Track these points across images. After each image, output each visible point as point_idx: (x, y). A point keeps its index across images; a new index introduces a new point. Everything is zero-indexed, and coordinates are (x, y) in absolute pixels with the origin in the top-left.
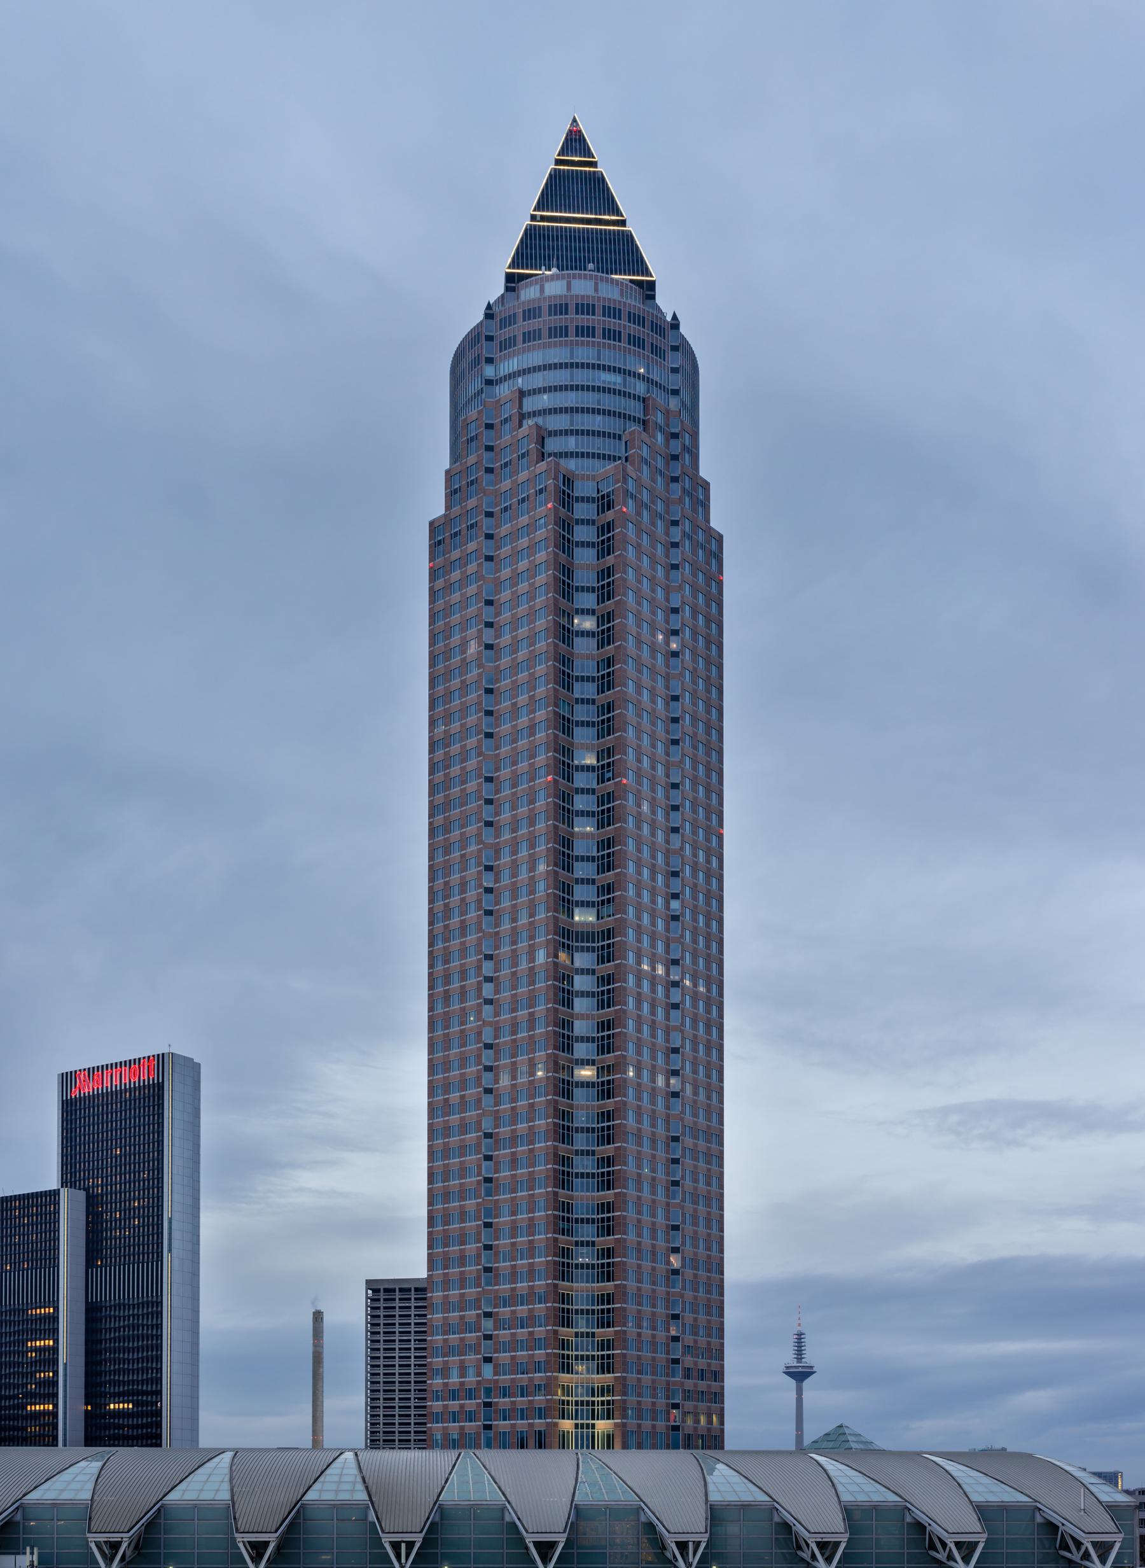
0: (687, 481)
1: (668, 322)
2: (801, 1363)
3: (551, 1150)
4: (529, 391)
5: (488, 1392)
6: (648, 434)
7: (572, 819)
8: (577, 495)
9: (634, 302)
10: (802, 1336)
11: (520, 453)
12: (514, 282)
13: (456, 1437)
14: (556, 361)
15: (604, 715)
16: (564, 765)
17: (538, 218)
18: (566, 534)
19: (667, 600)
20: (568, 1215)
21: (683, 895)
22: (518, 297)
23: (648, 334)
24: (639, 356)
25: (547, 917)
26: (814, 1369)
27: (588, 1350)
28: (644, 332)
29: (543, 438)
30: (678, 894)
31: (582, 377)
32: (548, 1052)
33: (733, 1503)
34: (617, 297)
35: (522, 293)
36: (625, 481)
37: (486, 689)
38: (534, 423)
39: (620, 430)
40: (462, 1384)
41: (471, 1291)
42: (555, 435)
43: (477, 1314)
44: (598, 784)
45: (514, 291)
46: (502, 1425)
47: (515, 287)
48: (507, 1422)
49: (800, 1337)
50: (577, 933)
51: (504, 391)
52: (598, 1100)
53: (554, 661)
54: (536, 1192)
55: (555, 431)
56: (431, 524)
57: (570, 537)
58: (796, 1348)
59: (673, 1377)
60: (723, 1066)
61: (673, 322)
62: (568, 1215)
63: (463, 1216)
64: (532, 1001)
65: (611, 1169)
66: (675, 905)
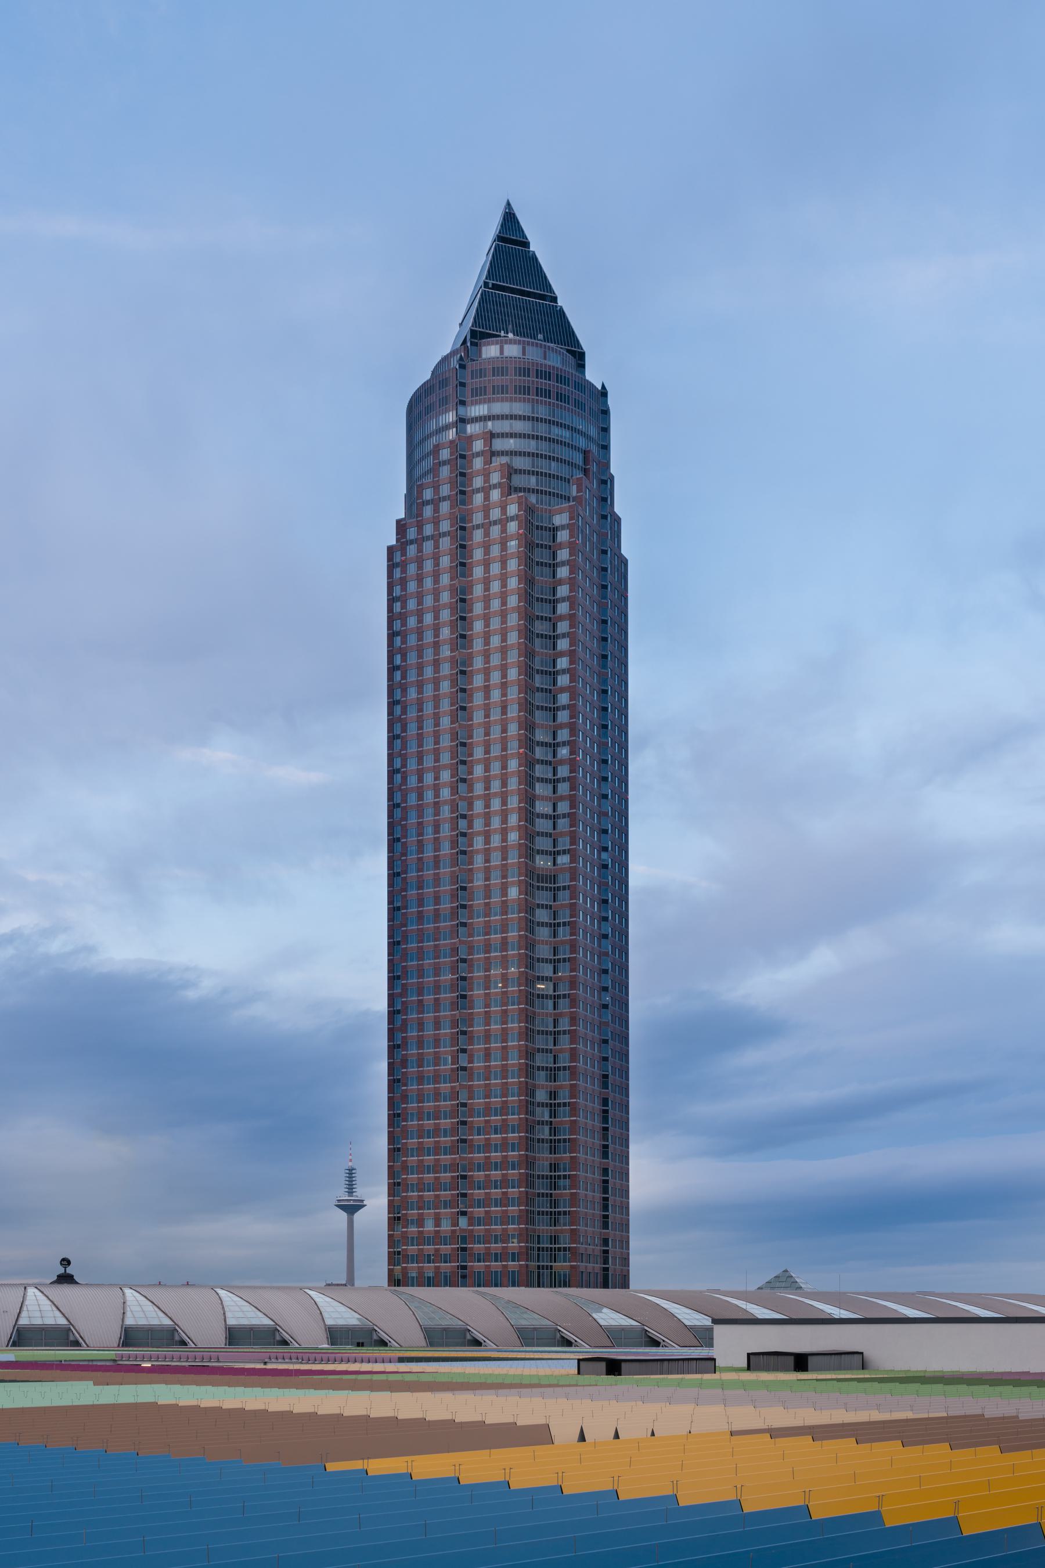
2: (352, 1196)
3: (524, 1049)
5: (464, 1239)
9: (571, 370)
10: (354, 1171)
13: (431, 1275)
14: (521, 413)
17: (490, 286)
24: (572, 412)
25: (519, 862)
26: (365, 1203)
27: (547, 1208)
28: (561, 388)
29: (511, 474)
32: (521, 970)
33: (344, 1327)
34: (559, 365)
35: (484, 349)
39: (569, 475)
40: (453, 1231)
41: (446, 1158)
45: (477, 346)
46: (478, 1266)
47: (477, 343)
51: (470, 429)
61: (603, 391)
63: (437, 1095)
64: (504, 928)
66: (604, 855)
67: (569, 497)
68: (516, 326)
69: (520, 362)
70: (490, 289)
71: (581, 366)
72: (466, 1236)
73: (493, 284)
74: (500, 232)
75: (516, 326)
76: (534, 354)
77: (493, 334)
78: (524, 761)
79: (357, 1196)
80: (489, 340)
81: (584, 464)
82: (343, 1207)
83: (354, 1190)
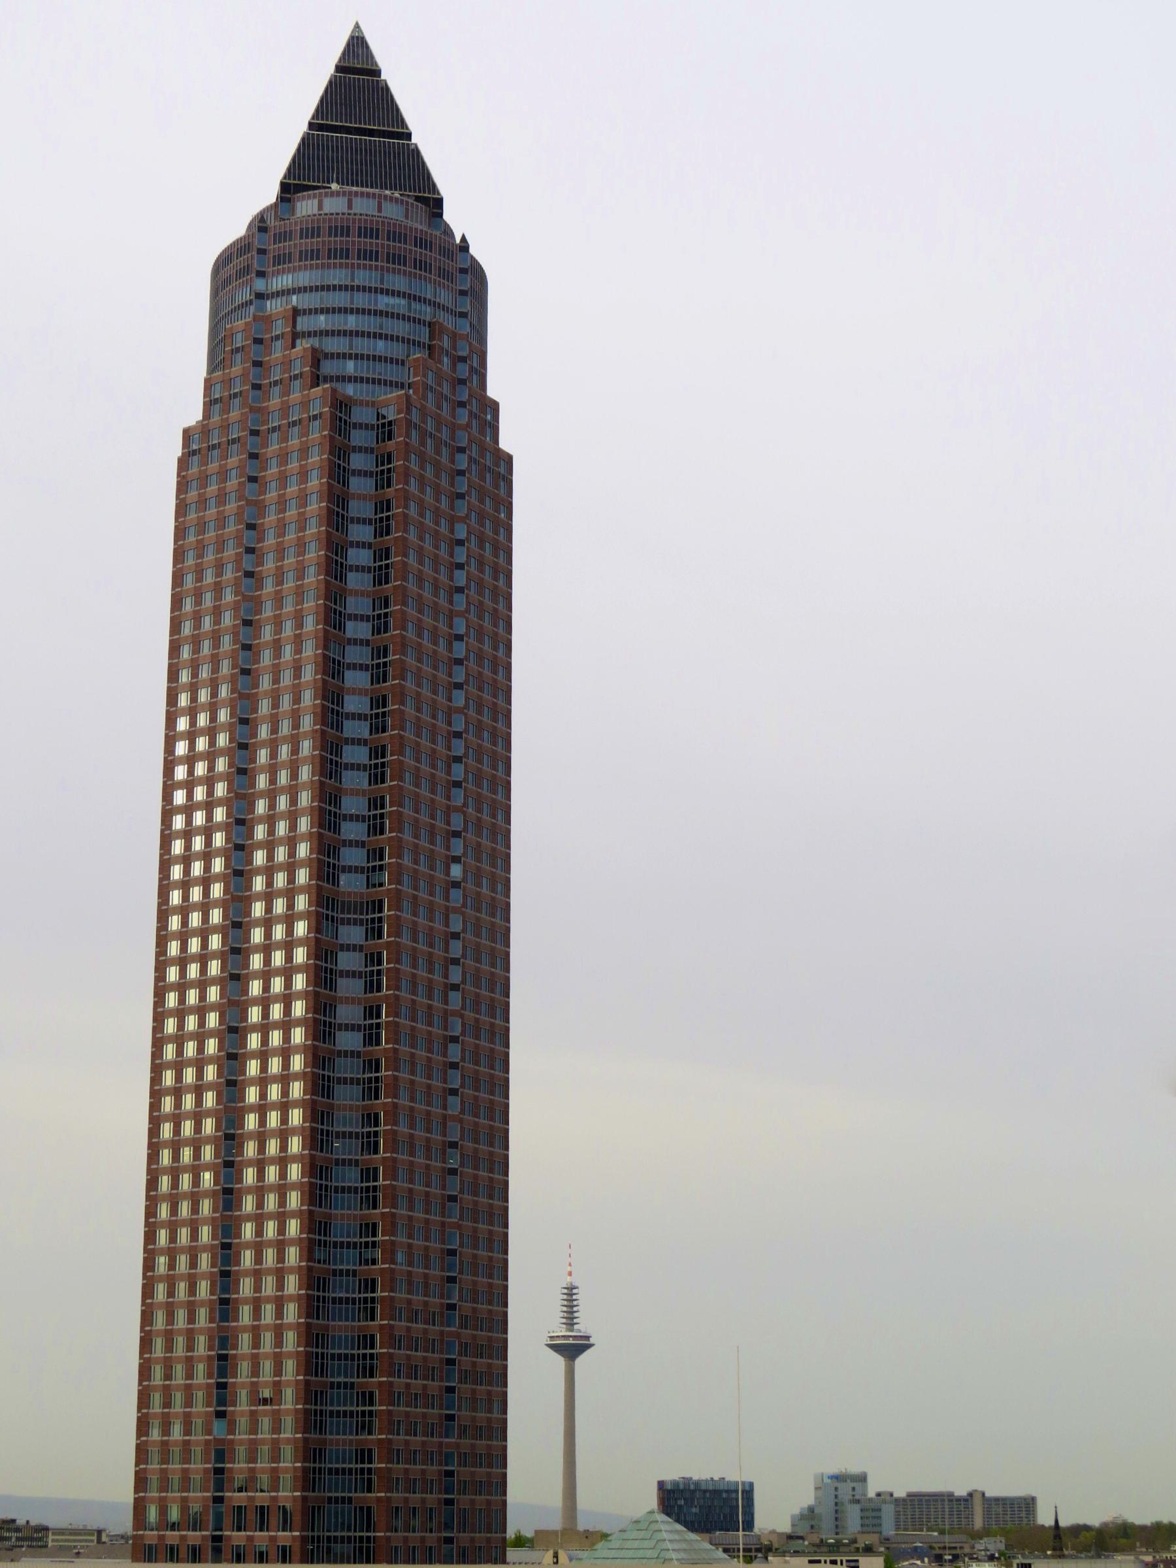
0: (475, 359)
1: (456, 245)
2: (572, 1331)
4: (305, 310)
7: (342, 722)
8: (346, 761)
9: (419, 224)
10: (575, 1291)
11: (292, 374)
12: (290, 193)
14: (336, 282)
15: (382, 561)
16: (339, 468)
18: (341, 462)
19: (452, 531)
20: (325, 1238)
21: (467, 589)
22: (293, 212)
23: (435, 258)
26: (592, 1341)
29: (319, 360)
30: (461, 758)
31: (361, 300)
35: (299, 204)
36: (408, 412)
37: (251, 430)
38: (309, 345)
43: (206, 1440)
44: (373, 635)
48: (243, 1533)
50: (343, 902)
51: (273, 306)
52: (363, 1100)
53: (321, 750)
56: (186, 432)
57: (347, 419)
58: (565, 1309)
59: (447, 1437)
60: (510, 734)
61: (463, 244)
62: (324, 1294)
65: (371, 1534)
68: (352, 174)
69: (336, 219)
72: (224, 1449)
75: (352, 174)
76: (364, 207)
77: (304, 185)
78: (318, 744)
79: (580, 1332)
80: (309, 192)
82: (555, 1348)
83: (575, 1321)
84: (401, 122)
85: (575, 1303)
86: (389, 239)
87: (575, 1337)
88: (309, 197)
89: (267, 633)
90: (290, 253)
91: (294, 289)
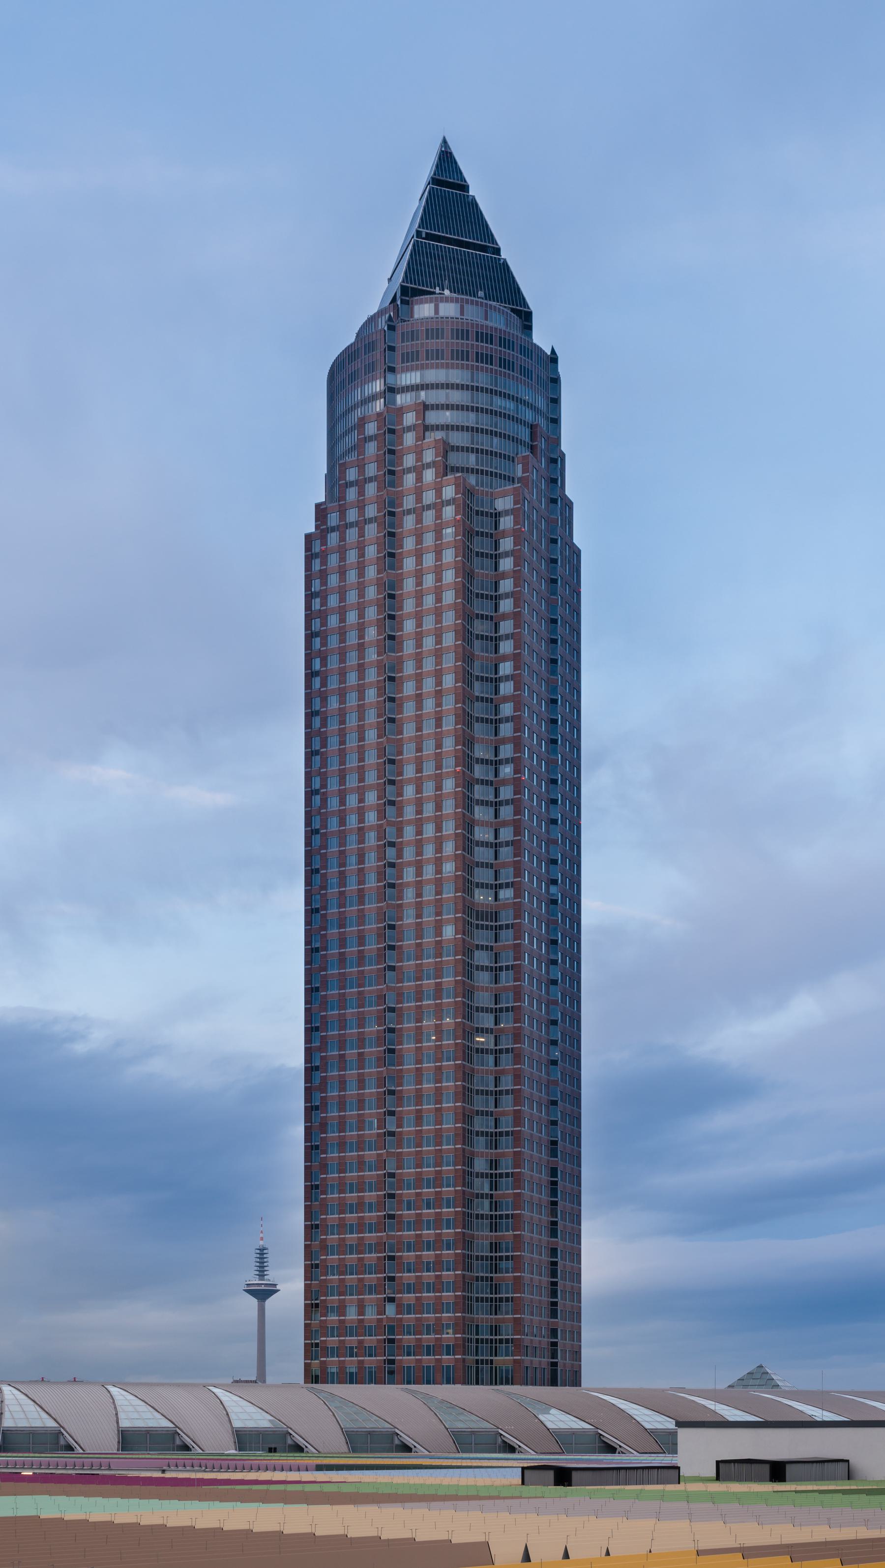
1: (548, 356)
2: (264, 1280)
3: (460, 1111)
4: (432, 405)
6: (536, 458)
9: (515, 331)
14: (458, 381)
17: (424, 235)
26: (278, 1287)
29: (447, 452)
35: (416, 307)
42: (458, 450)
49: (262, 1253)
50: (477, 912)
54: (443, 1147)
55: (458, 447)
61: (553, 356)
64: (439, 972)
66: (553, 889)
67: (513, 478)
70: (423, 239)
71: (528, 327)
73: (427, 233)
74: (435, 174)
80: (422, 297)
81: (531, 441)
83: (265, 1273)
84: (491, 238)
85: (265, 1260)
86: (477, 341)
87: (266, 1285)
88: (426, 302)
89: (409, 688)
90: (418, 352)
91: (422, 385)
